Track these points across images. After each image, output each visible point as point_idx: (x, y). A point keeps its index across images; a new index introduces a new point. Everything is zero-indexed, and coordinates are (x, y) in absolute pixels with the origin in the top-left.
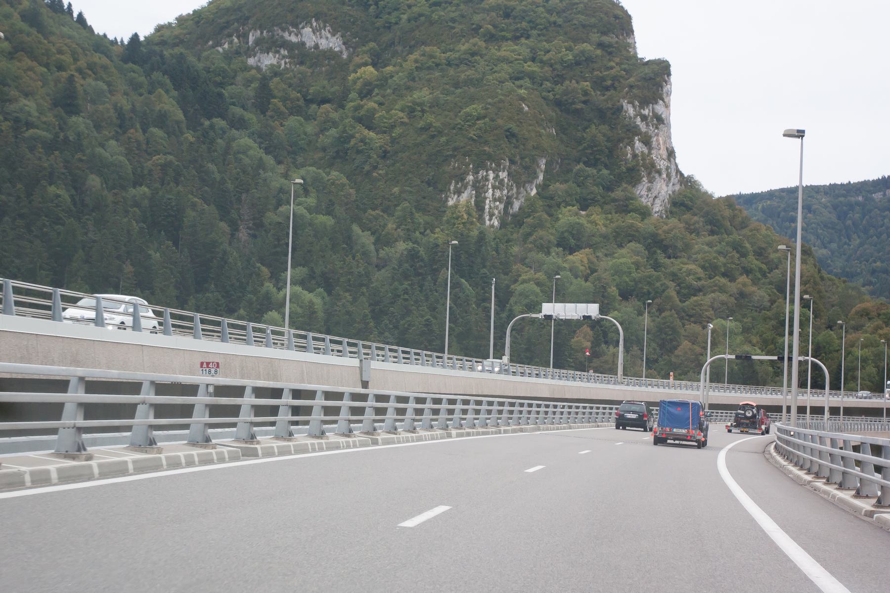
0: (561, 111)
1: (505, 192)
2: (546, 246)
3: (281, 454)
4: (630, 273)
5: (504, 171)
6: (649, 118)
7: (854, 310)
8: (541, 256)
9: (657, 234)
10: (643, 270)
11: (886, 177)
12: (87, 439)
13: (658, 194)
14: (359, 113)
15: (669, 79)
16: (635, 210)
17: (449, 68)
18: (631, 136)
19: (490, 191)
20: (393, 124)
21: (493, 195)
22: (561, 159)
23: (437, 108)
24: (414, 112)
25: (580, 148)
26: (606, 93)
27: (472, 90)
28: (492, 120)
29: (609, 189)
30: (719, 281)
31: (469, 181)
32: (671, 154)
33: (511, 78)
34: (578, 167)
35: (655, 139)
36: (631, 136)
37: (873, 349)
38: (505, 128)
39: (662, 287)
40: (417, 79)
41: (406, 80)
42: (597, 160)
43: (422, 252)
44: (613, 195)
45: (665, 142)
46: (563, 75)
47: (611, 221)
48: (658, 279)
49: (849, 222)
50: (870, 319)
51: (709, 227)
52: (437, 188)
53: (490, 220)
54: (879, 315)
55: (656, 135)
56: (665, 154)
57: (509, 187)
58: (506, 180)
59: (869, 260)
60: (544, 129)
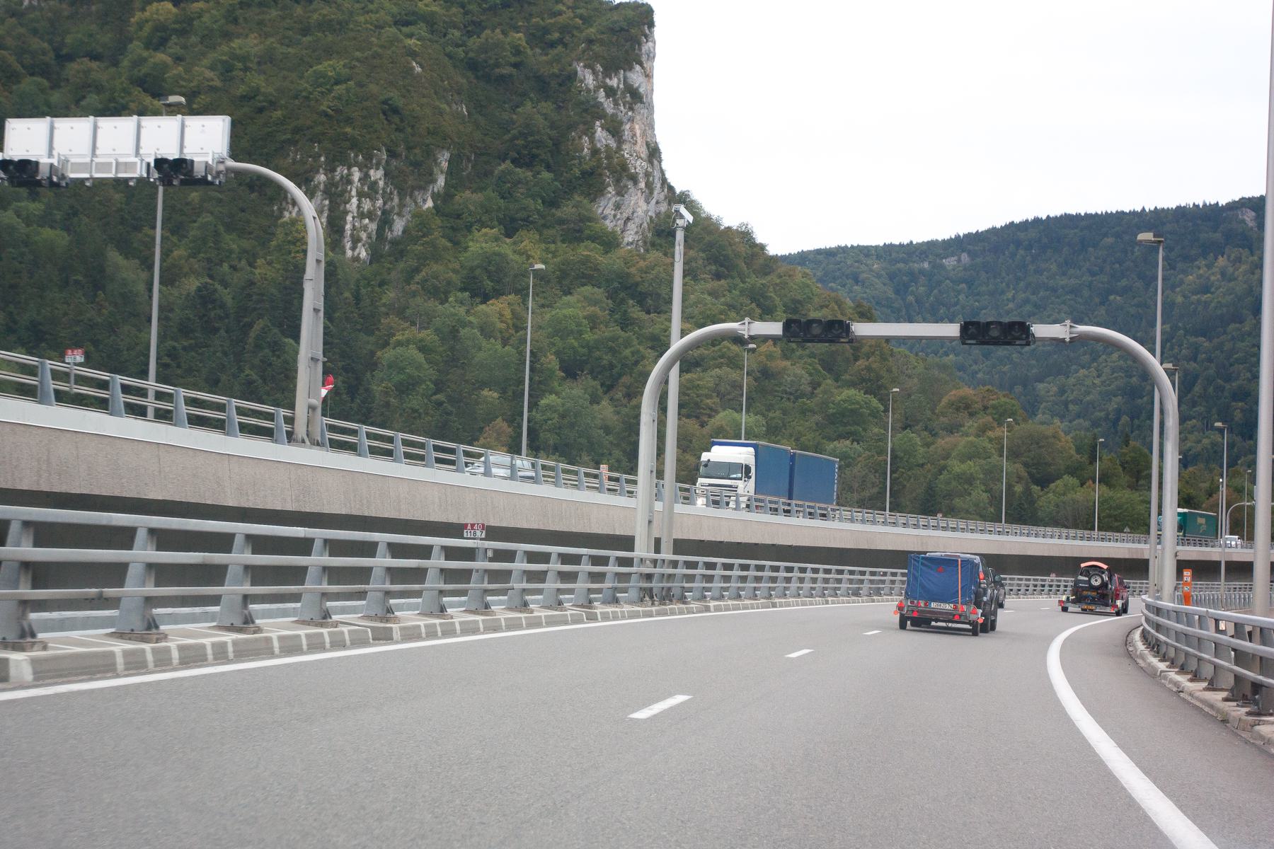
0: (477, 77)
1: (380, 203)
2: (442, 290)
3: (509, 628)
4: (580, 333)
5: (377, 169)
6: (619, 93)
7: (945, 401)
8: (432, 304)
9: (628, 275)
10: (604, 329)
11: (961, 235)
12: (38, 621)
13: (633, 213)
14: (139, 71)
15: (652, 33)
16: (594, 238)
17: (296, 5)
18: (589, 120)
19: (354, 201)
20: (195, 89)
21: (359, 207)
22: (475, 154)
23: (269, 65)
24: (231, 71)
25: (507, 137)
26: (551, 51)
27: (330, 38)
28: (360, 85)
29: (553, 203)
30: (729, 349)
31: (319, 183)
32: (654, 153)
33: (396, 23)
34: (503, 167)
35: (628, 127)
36: (589, 120)
37: (983, 462)
38: (382, 98)
39: (633, 356)
40: (241, 20)
41: (223, 21)
42: (534, 157)
43: (226, 295)
44: (558, 213)
45: (644, 134)
46: (481, 21)
47: (554, 254)
48: (627, 344)
49: (911, 298)
50: (971, 415)
51: (714, 268)
52: (265, 195)
53: (353, 249)
54: (985, 408)
55: (629, 120)
56: (644, 152)
57: (387, 196)
58: (381, 183)
59: (938, 352)
60: (448, 104)
